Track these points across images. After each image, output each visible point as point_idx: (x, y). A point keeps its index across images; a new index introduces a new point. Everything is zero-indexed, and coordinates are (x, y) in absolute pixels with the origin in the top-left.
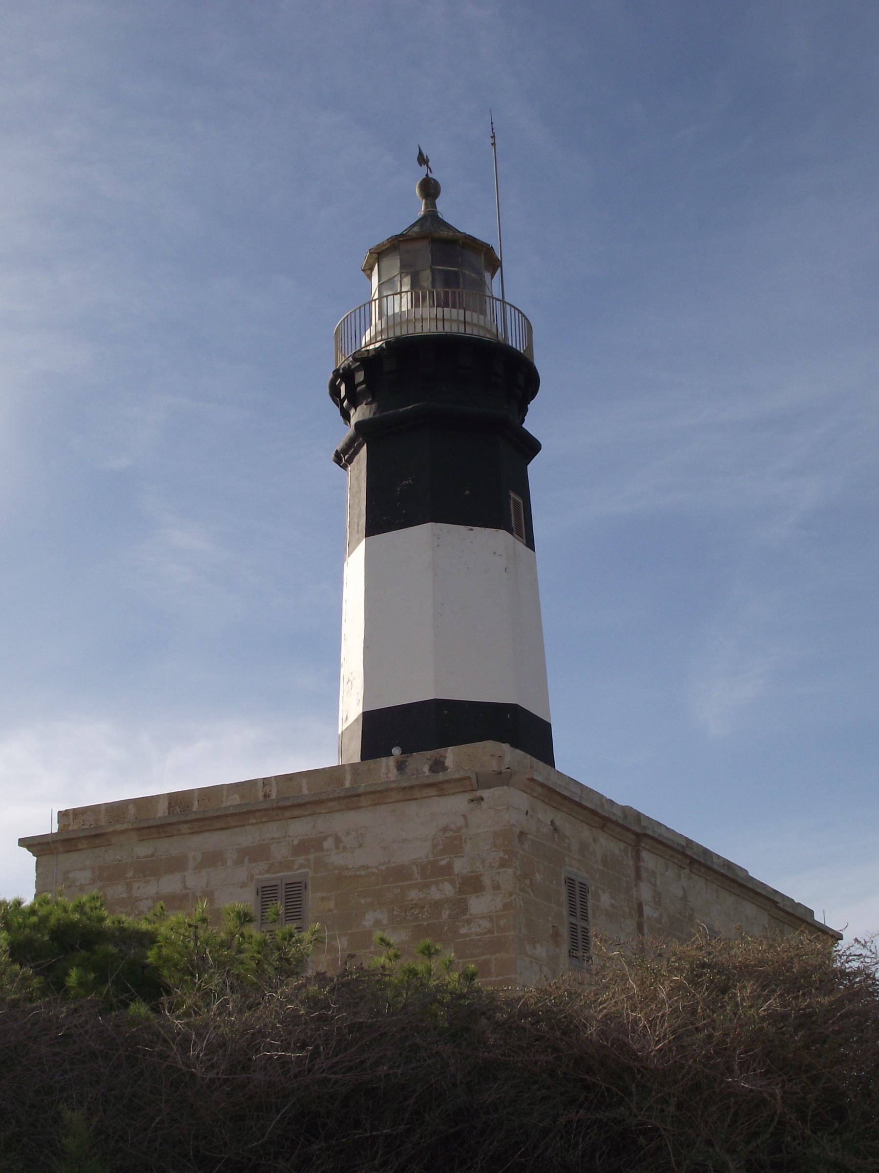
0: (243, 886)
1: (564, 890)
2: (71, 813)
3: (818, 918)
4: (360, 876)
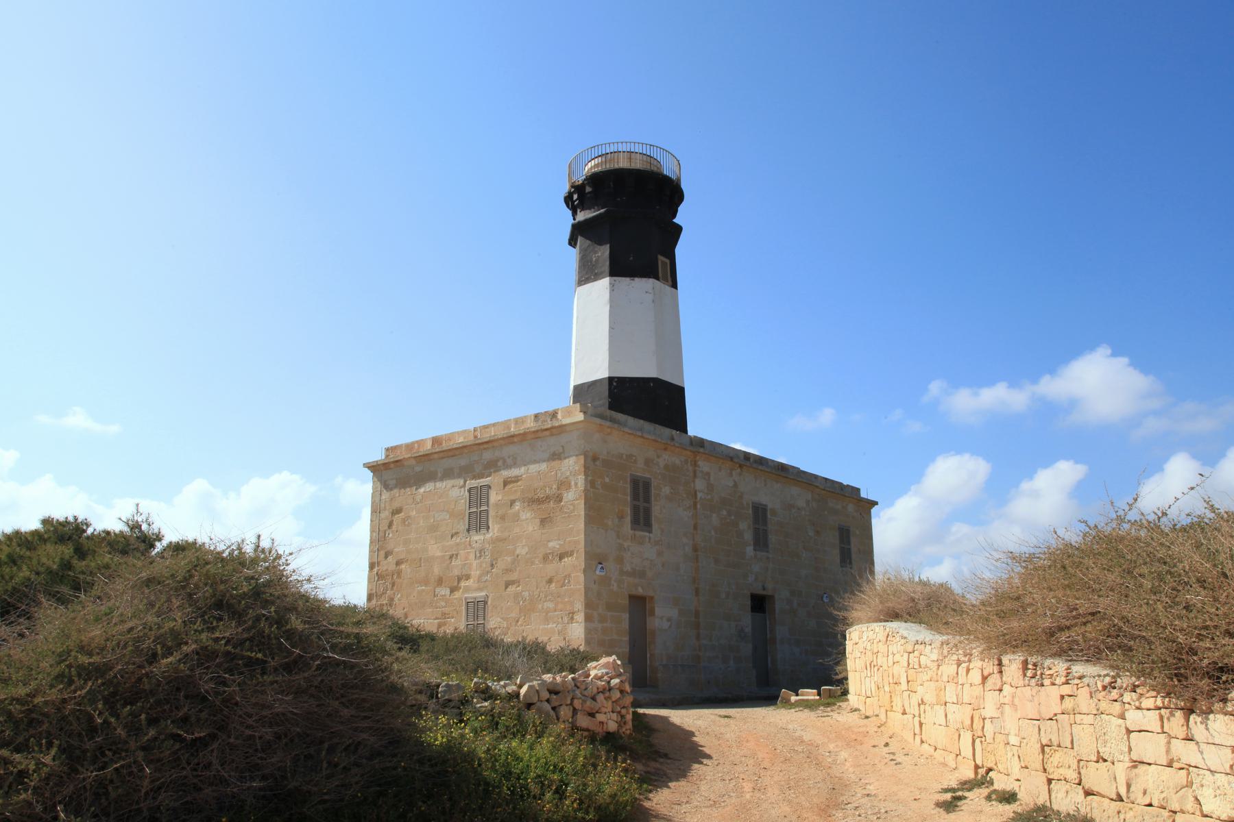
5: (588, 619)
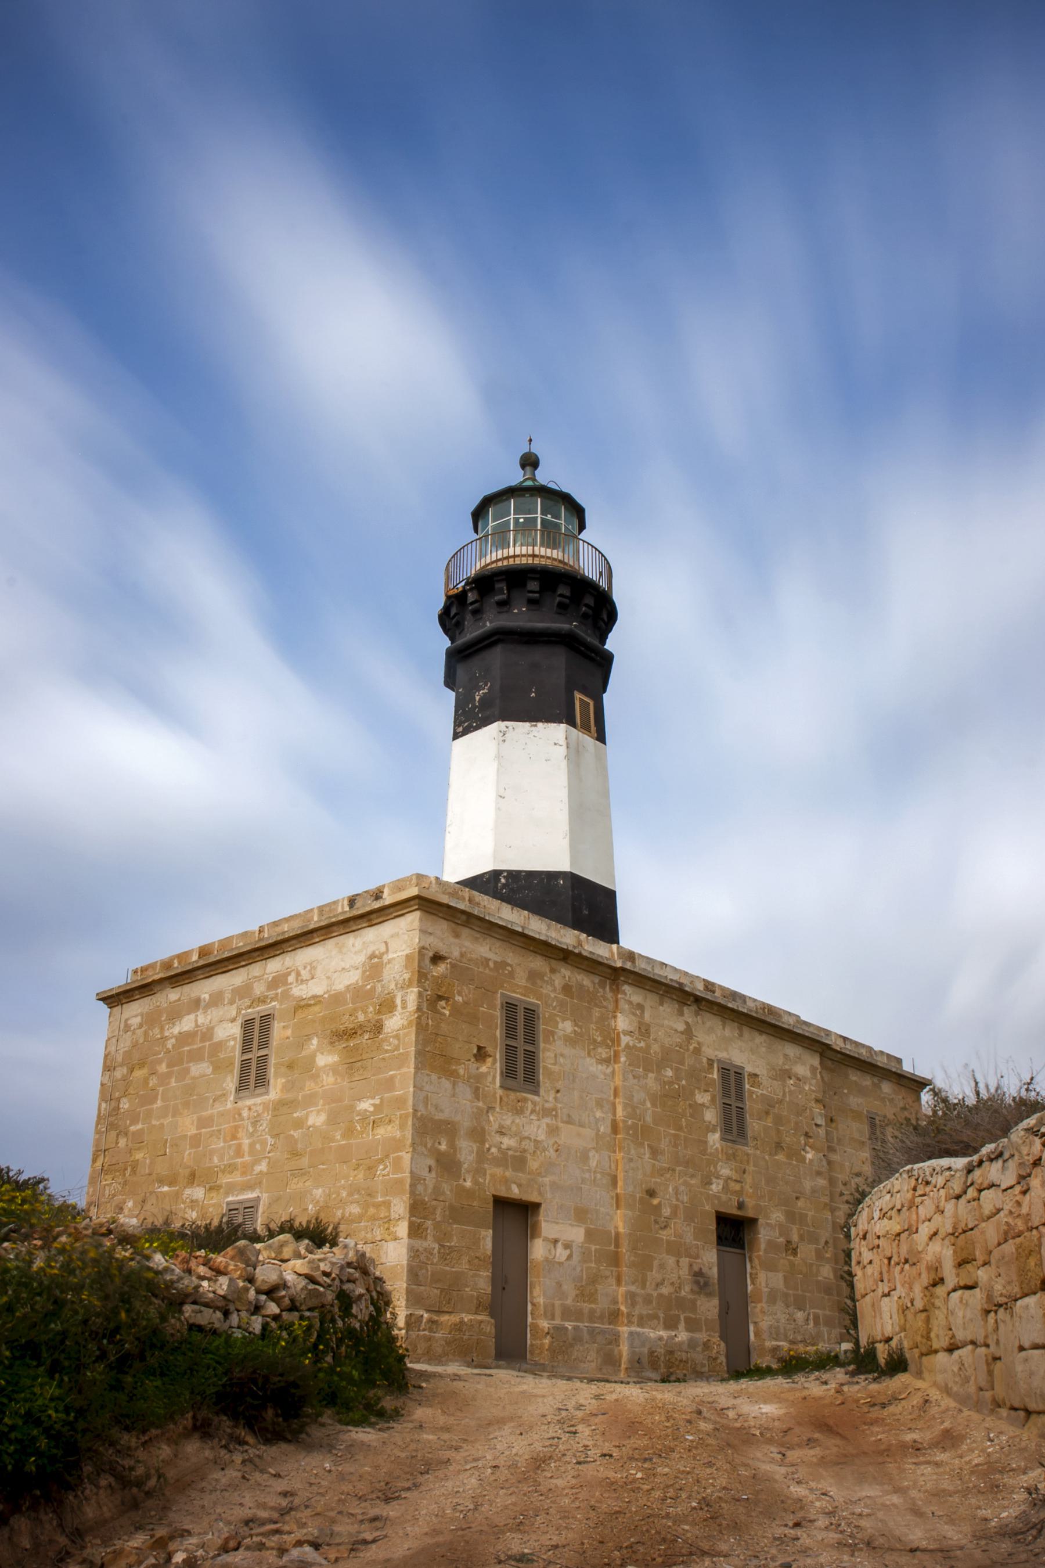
0: (233, 1020)
1: (498, 1014)
3: (907, 1067)
4: (310, 1005)
5: (415, 1231)
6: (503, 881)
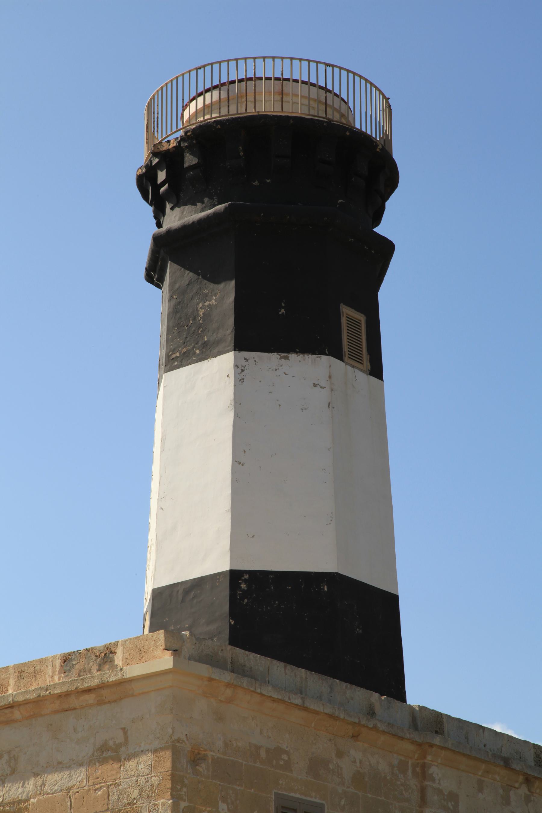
2: (11, 671)
6: (243, 586)
